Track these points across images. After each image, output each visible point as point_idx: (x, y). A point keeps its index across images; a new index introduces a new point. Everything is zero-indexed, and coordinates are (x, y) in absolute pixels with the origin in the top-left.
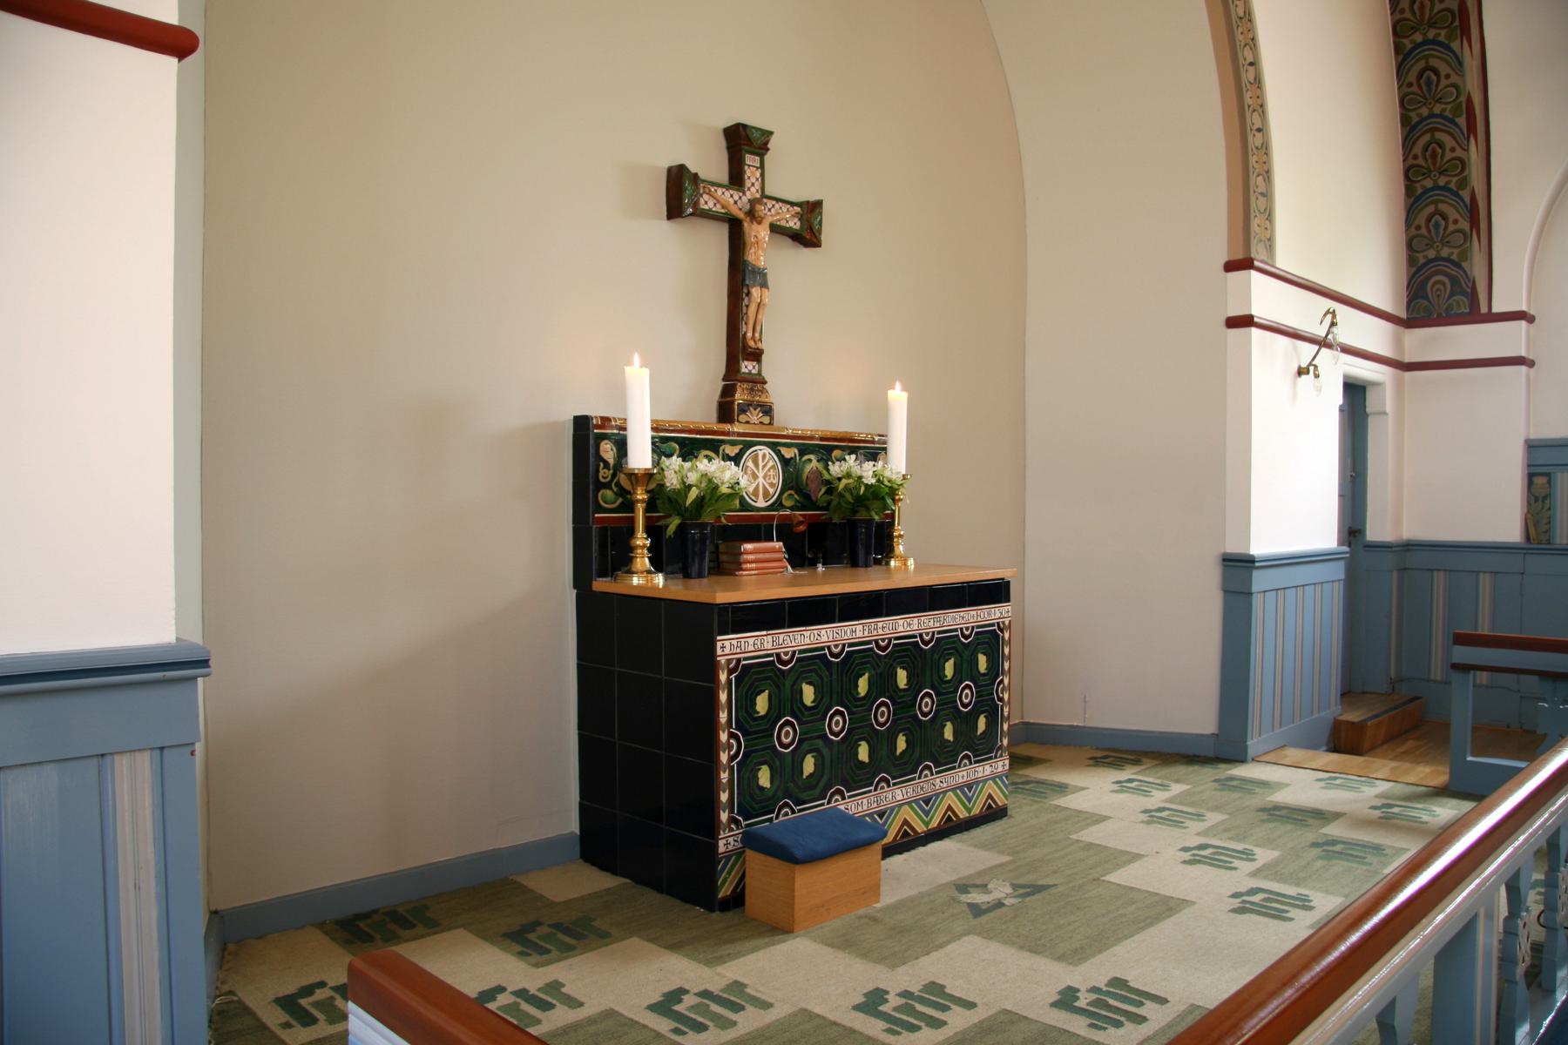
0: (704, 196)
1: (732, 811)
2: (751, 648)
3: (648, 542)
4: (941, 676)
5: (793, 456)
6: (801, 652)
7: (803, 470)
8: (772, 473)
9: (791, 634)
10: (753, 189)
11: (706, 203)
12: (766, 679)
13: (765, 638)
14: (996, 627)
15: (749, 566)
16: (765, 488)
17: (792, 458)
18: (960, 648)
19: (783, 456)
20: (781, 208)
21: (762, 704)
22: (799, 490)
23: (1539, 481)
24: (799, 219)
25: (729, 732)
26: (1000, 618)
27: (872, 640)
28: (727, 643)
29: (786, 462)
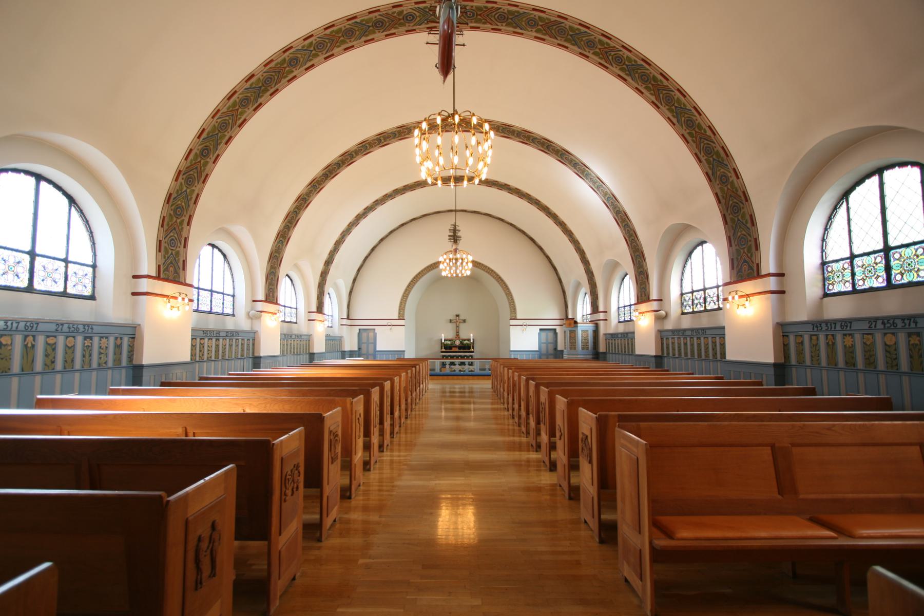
23: (237, 341)
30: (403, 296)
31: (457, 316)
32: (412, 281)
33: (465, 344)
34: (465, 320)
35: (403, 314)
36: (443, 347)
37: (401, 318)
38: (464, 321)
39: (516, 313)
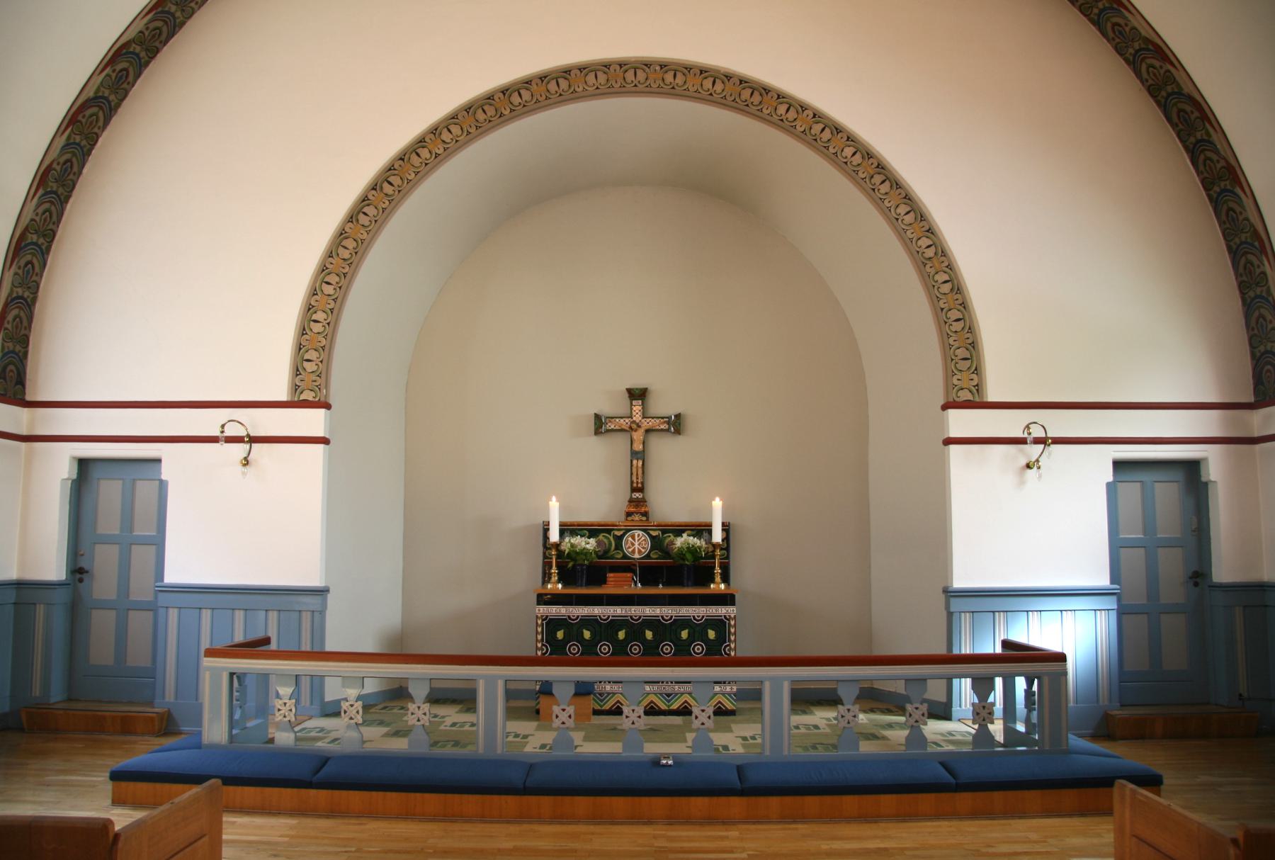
0: (609, 424)
4: (679, 638)
6: (582, 616)
8: (644, 542)
14: (723, 617)
17: (656, 536)
19: (651, 535)
21: (560, 635)
28: (541, 609)
29: (652, 537)
30: (323, 269)
31: (638, 395)
32: (374, 187)
33: (681, 554)
34: (678, 416)
35: (323, 374)
36: (554, 570)
37: (308, 396)
38: (676, 425)
39: (977, 371)
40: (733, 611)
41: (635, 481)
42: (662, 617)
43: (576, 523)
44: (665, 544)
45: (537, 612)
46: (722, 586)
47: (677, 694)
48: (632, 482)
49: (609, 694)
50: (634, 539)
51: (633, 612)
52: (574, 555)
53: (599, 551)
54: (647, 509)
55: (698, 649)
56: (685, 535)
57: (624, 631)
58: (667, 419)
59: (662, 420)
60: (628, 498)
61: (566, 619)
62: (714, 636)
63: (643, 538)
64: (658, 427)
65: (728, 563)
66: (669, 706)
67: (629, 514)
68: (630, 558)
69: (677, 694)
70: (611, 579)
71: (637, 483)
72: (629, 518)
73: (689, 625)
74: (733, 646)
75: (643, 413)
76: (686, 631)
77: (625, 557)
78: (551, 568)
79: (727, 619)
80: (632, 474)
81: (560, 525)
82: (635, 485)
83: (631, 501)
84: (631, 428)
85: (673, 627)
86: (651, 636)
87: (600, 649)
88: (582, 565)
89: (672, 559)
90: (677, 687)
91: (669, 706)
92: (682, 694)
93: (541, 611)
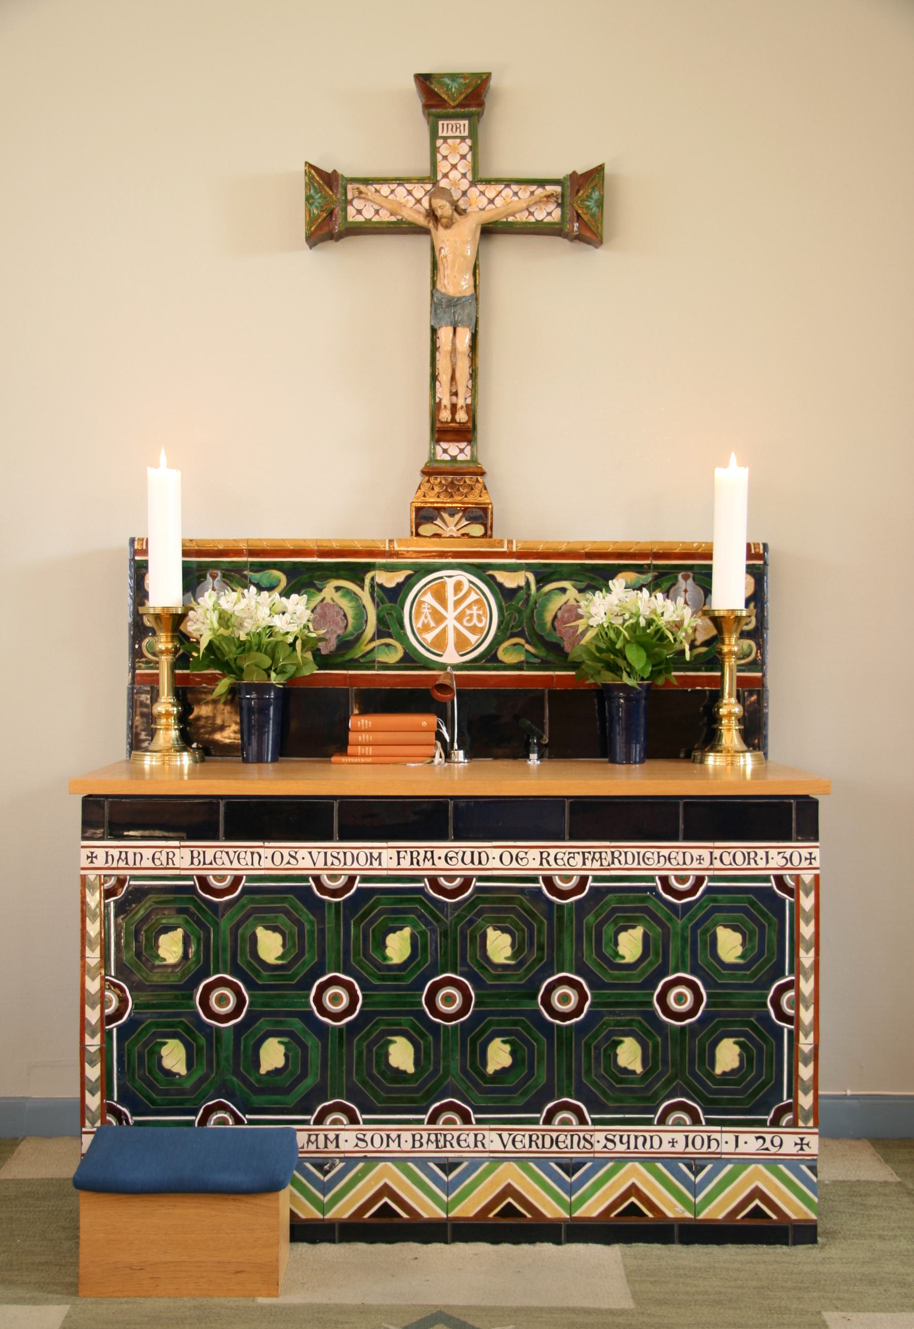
0: (356, 203)
1: (107, 1093)
2: (147, 863)
3: (175, 710)
4: (611, 962)
5: (523, 584)
6: (251, 878)
7: (544, 607)
8: (475, 611)
9: (231, 851)
10: (455, 175)
11: (359, 212)
12: (247, 917)
13: (176, 851)
15: (360, 749)
16: (458, 634)
17: (519, 588)
18: (662, 912)
19: (500, 586)
20: (516, 194)
22: (537, 639)
24: (559, 205)
25: (103, 978)
26: (782, 868)
27: (424, 876)
29: (506, 595)
40: (811, 858)
41: (446, 401)
42: (548, 880)
43: (243, 546)
44: (548, 617)
45: (85, 863)
46: (747, 761)
47: (599, 1163)
48: (436, 407)
49: (350, 1162)
50: (441, 599)
51: (441, 864)
52: (231, 653)
53: (320, 639)
54: (485, 499)
55: (680, 998)
56: (618, 584)
57: (407, 931)
58: (558, 189)
59: (539, 192)
60: (422, 461)
61: (193, 887)
62: (739, 951)
63: (473, 597)
64: (522, 217)
65: (761, 682)
66: (570, 1208)
67: (424, 515)
68: (426, 665)
69: (599, 1163)
70: (363, 737)
71: (454, 408)
72: (427, 529)
73: (647, 910)
74: (806, 987)
75: (475, 169)
76: (637, 933)
77: (410, 659)
78: (155, 696)
79: (790, 892)
80: (434, 378)
81: (185, 553)
82: (445, 415)
83: (429, 472)
84: (432, 214)
85: (590, 919)
86: (508, 952)
87: (318, 1000)
88: (262, 688)
89: (575, 666)
90: (600, 1136)
91: (570, 1208)
92: (622, 1161)
93: (100, 862)
